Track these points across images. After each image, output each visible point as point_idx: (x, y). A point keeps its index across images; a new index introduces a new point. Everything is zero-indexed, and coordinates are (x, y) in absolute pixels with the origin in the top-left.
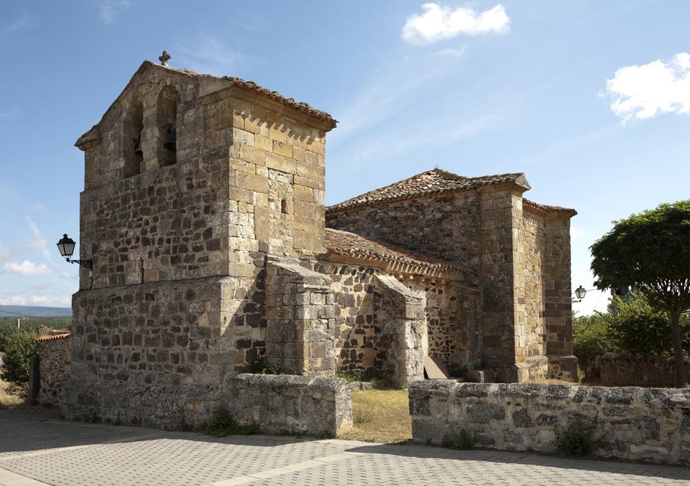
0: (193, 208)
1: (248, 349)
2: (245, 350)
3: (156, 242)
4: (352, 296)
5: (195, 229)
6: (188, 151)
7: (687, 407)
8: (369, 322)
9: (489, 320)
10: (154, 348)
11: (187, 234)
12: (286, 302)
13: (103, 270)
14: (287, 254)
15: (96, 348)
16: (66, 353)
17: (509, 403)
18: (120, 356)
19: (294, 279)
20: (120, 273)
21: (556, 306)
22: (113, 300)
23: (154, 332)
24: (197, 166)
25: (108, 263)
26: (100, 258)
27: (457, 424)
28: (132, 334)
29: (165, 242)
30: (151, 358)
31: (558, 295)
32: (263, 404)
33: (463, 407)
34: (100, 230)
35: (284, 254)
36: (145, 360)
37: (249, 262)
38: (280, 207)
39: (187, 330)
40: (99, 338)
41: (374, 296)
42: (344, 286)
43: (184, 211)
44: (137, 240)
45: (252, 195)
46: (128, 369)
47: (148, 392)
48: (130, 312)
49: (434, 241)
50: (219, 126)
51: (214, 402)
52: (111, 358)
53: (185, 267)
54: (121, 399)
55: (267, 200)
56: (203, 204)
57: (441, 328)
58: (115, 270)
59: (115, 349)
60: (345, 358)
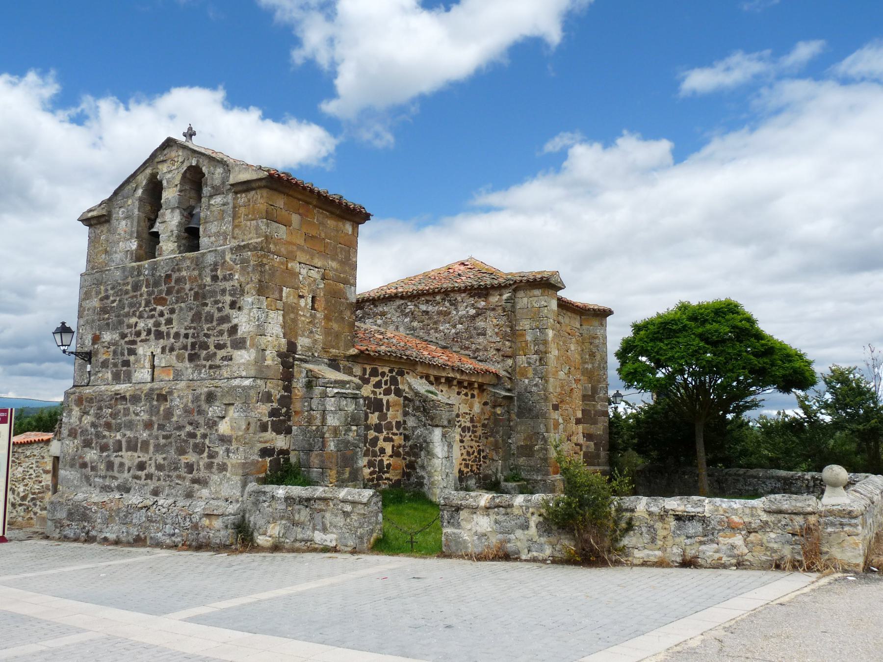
0: (216, 302)
1: (272, 458)
2: (268, 459)
3: (172, 337)
4: (381, 400)
5: (218, 325)
6: (213, 239)
7: (677, 513)
8: (398, 429)
9: (523, 428)
10: (164, 456)
11: (208, 329)
12: (314, 407)
13: (105, 364)
14: (316, 354)
15: (91, 455)
16: (45, 460)
17: (533, 514)
18: (122, 465)
19: (324, 383)
20: (124, 368)
21: (593, 412)
22: (116, 399)
23: (165, 437)
24: (223, 257)
25: (111, 357)
26: (102, 350)
27: (486, 535)
28: (138, 439)
29: (181, 337)
30: (160, 467)
31: (594, 401)
32: (288, 519)
33: (491, 518)
34: (103, 319)
35: (313, 354)
36: (152, 470)
37: (276, 363)
38: (310, 304)
39: (204, 436)
40: (97, 443)
41: (404, 401)
42: (373, 389)
43: (206, 305)
44: (149, 332)
45: (281, 291)
46: (130, 479)
47: (155, 506)
48: (137, 414)
49: (467, 339)
50: (250, 216)
51: (233, 517)
52: (110, 466)
53: (205, 366)
54: (121, 515)
55: (297, 297)
56: (228, 299)
57: (473, 435)
58: (120, 365)
59: (116, 456)
60: (372, 469)
